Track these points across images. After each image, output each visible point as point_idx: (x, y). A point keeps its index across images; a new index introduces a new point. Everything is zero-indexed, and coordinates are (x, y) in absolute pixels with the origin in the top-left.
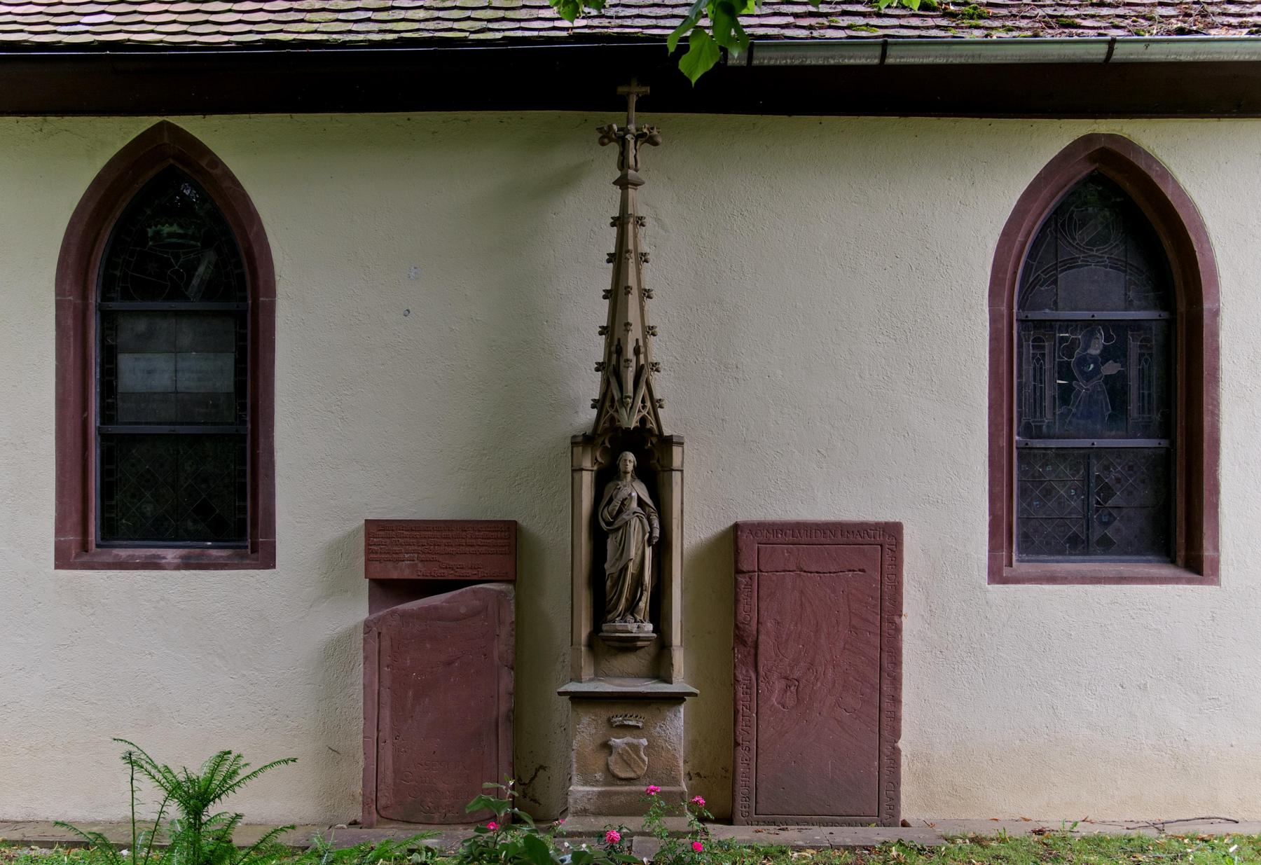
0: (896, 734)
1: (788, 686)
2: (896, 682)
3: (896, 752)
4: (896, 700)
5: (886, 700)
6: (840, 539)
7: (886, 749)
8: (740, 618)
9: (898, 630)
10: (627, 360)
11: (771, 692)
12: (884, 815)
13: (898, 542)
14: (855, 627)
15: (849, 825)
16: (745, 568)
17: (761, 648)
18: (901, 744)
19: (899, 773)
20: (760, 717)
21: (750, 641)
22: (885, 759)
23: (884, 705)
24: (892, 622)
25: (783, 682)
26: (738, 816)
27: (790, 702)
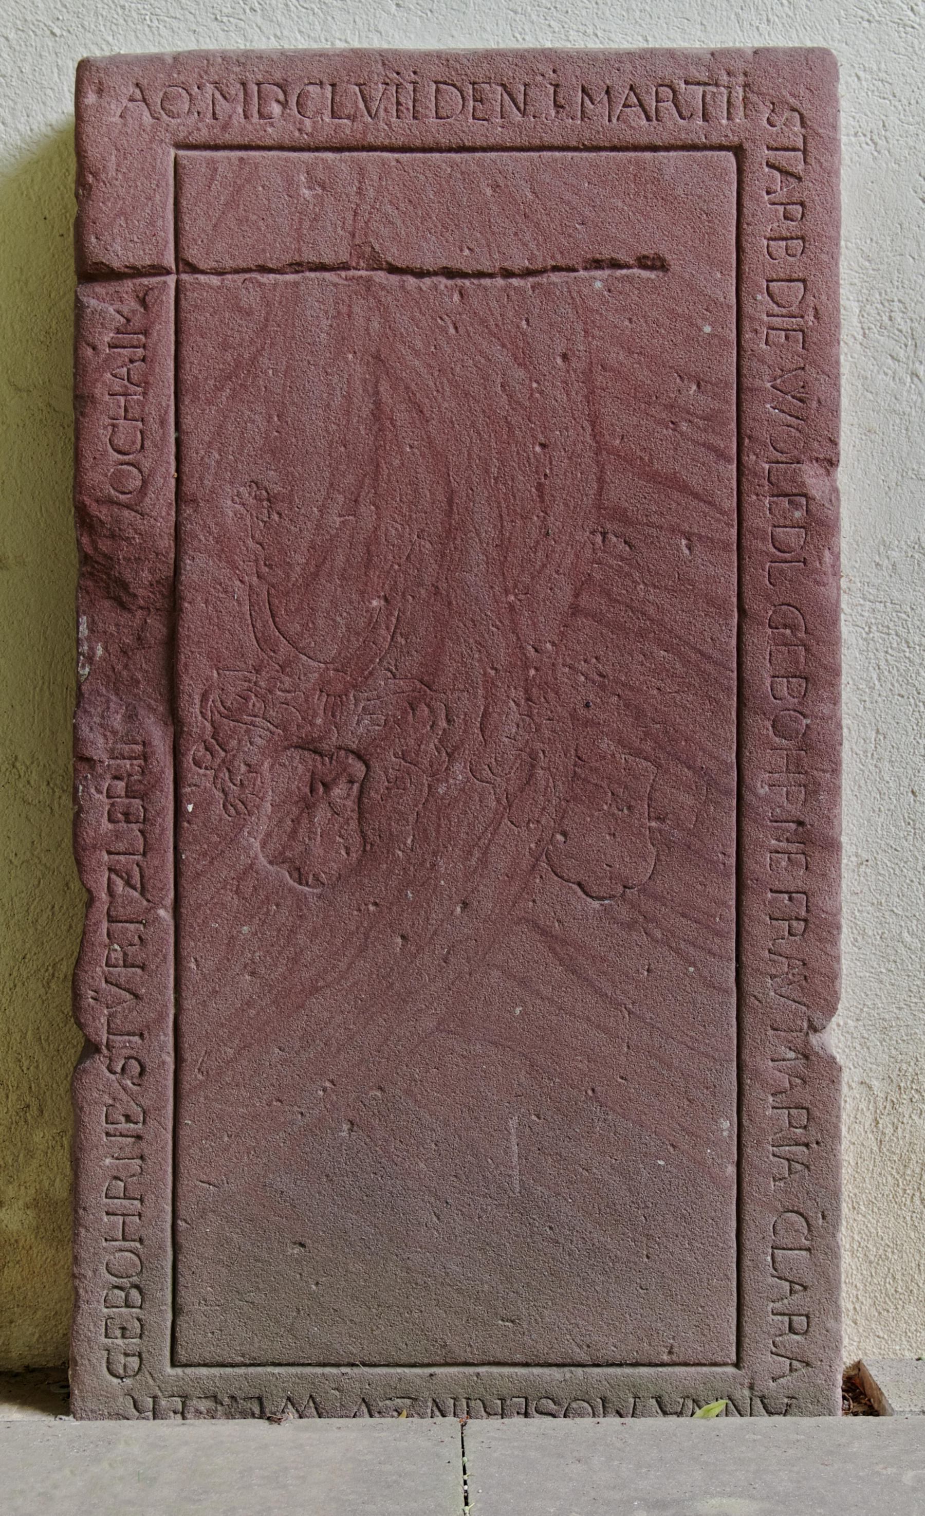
0: (816, 990)
1: (319, 784)
2: (813, 756)
3: (817, 1071)
4: (814, 841)
5: (766, 841)
6: (555, 127)
7: (772, 1062)
8: (95, 477)
9: (819, 525)
10: (113, 1343)
11: (241, 809)
12: (763, 1360)
13: (812, 141)
14: (621, 515)
15: (606, 1406)
16: (117, 251)
17: (194, 611)
18: (837, 1039)
19: (832, 1168)
20: (191, 921)
21: (143, 580)
22: (764, 1106)
23: (761, 864)
24: (797, 495)
25: (299, 765)
26: (92, 1375)
27: (331, 854)
